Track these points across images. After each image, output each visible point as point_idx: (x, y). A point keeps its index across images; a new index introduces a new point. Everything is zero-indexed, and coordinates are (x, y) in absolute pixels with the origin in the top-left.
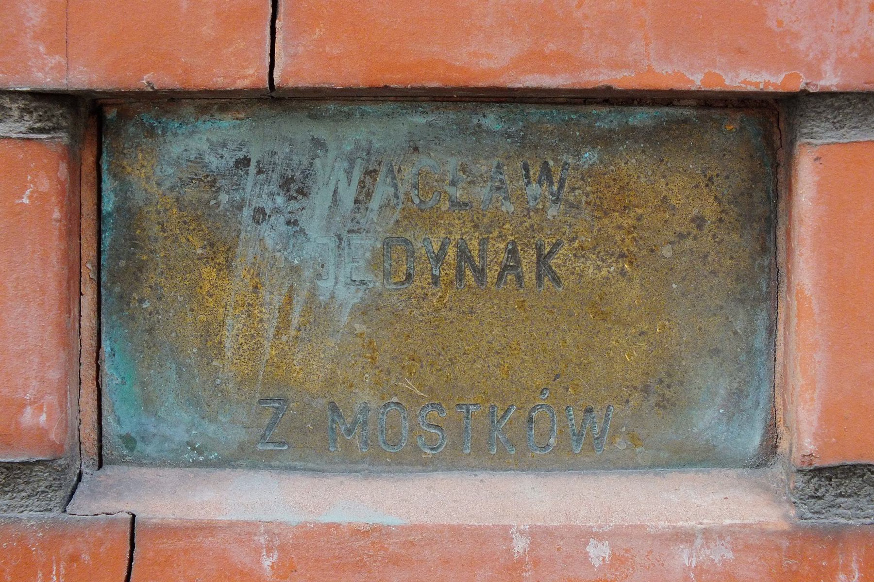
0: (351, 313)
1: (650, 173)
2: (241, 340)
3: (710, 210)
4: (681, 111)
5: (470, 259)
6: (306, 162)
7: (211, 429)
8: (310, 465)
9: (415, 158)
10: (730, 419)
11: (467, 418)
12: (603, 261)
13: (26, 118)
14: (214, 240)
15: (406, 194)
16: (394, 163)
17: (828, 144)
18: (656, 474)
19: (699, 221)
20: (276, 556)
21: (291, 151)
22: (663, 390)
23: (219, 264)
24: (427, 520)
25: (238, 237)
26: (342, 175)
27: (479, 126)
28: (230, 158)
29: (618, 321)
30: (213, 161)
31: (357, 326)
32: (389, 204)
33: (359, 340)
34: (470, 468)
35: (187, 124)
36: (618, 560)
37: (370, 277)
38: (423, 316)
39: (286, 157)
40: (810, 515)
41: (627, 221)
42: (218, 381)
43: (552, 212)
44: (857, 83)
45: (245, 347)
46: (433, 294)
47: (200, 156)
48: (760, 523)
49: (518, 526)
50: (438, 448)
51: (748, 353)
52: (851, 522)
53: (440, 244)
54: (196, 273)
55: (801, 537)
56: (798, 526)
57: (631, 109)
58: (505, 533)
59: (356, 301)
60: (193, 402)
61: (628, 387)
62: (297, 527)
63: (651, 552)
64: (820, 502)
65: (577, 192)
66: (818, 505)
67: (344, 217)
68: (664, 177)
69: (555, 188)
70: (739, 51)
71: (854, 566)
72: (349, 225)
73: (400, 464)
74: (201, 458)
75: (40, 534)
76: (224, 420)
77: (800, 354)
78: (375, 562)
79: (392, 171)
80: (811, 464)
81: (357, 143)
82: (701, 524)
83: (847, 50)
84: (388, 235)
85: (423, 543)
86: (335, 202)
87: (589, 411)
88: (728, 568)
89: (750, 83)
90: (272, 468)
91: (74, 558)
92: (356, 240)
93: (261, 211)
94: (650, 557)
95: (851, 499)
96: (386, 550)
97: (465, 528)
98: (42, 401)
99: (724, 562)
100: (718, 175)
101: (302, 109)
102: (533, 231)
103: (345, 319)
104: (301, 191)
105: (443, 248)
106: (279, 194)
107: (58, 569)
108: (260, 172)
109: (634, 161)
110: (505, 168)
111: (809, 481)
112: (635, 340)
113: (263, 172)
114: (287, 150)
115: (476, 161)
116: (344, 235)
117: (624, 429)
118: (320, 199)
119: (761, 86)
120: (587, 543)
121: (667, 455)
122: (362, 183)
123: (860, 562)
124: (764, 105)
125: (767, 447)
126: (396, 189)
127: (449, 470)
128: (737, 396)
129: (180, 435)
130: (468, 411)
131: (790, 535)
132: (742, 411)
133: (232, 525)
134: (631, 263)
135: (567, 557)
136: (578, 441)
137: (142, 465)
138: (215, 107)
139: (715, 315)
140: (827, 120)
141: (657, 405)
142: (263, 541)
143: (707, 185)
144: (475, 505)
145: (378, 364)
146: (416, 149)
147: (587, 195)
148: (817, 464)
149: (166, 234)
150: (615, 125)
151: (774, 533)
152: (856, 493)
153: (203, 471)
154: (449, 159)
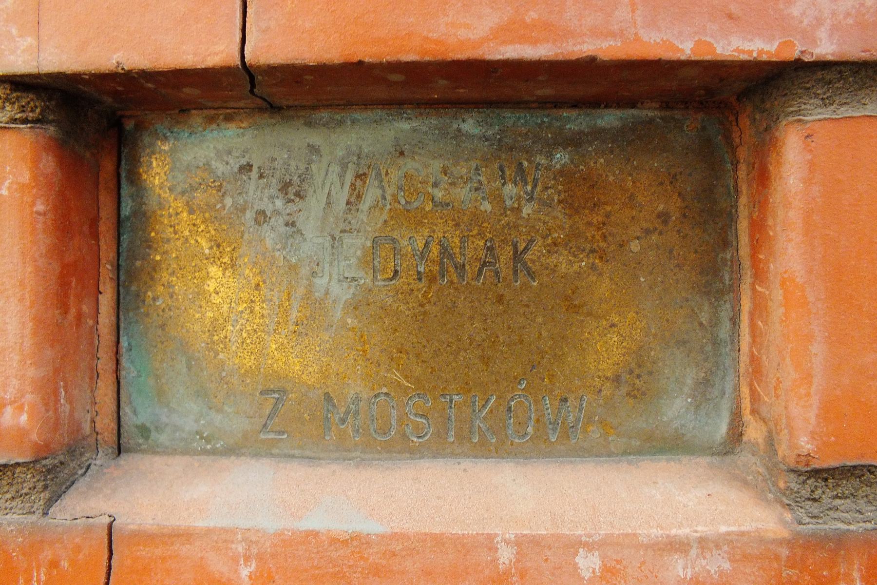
0: (344, 308)
1: (617, 172)
2: (245, 335)
3: (674, 206)
4: (645, 112)
5: (451, 257)
6: (302, 167)
7: (218, 418)
8: (308, 453)
9: (401, 161)
10: (697, 407)
11: (451, 407)
12: (575, 256)
13: (7, 108)
14: (220, 240)
15: (393, 196)
16: (381, 168)
17: (819, 120)
18: (630, 463)
19: (664, 217)
20: (254, 565)
21: (289, 157)
22: (637, 381)
23: (225, 263)
24: (410, 526)
25: (242, 237)
26: (336, 180)
27: (459, 130)
28: (235, 164)
29: (589, 314)
30: (220, 168)
31: (349, 321)
32: (377, 205)
33: (350, 334)
34: (453, 455)
35: (196, 133)
36: (609, 572)
37: (361, 274)
38: (409, 310)
39: (284, 163)
40: (808, 520)
41: (596, 219)
42: (224, 374)
43: (527, 210)
44: (854, 51)
45: (248, 341)
46: (418, 290)
47: (208, 164)
48: (757, 530)
49: (503, 534)
50: (424, 436)
51: (714, 344)
52: (852, 527)
53: (424, 242)
54: (204, 272)
55: (804, 547)
56: (798, 533)
57: (599, 111)
58: (489, 543)
59: (348, 296)
60: (201, 394)
61: (600, 377)
62: (275, 534)
63: (643, 563)
64: (816, 504)
65: (550, 191)
66: (815, 509)
67: (337, 218)
68: (631, 175)
69: (529, 188)
70: (730, 16)
71: (856, 575)
72: (342, 226)
73: (389, 452)
74: (209, 447)
75: (20, 539)
76: (229, 410)
77: (790, 346)
78: (355, 573)
79: (380, 174)
80: (807, 465)
81: (348, 148)
82: (696, 531)
83: (841, 17)
84: (377, 234)
85: (404, 553)
86: (328, 204)
87: (565, 400)
88: (724, 579)
89: (744, 52)
90: (273, 455)
91: (54, 564)
92: (347, 240)
93: (262, 213)
94: (643, 568)
95: (848, 501)
96: (366, 560)
97: (447, 537)
98: (23, 400)
99: (721, 573)
100: (681, 173)
101: (299, 117)
102: (510, 228)
103: (339, 314)
104: (298, 194)
105: (427, 244)
106: (278, 198)
107: (38, 575)
108: (261, 176)
109: (602, 160)
110: (484, 169)
111: (804, 482)
112: (606, 332)
113: (264, 177)
114: (286, 156)
115: (455, 164)
116: (337, 235)
117: (597, 418)
118: (315, 203)
119: (755, 55)
120: (576, 554)
121: (638, 443)
122: (353, 186)
123: (862, 571)
124: (722, 105)
125: (734, 434)
126: (384, 191)
127: (434, 457)
128: (705, 383)
129: (189, 425)
130: (451, 401)
131: (788, 543)
132: (709, 399)
133: (209, 532)
134: (601, 258)
135: (555, 568)
136: (554, 430)
137: (155, 453)
138: (221, 117)
139: (681, 307)
140: (816, 96)
141: (628, 394)
142: (240, 549)
143: (671, 183)
144: (459, 503)
145: (368, 356)
146: (402, 153)
147: (559, 193)
148: (816, 465)
149: (177, 236)
150: (584, 127)
151: (774, 541)
152: (852, 494)
153: (208, 460)
154: (432, 162)
